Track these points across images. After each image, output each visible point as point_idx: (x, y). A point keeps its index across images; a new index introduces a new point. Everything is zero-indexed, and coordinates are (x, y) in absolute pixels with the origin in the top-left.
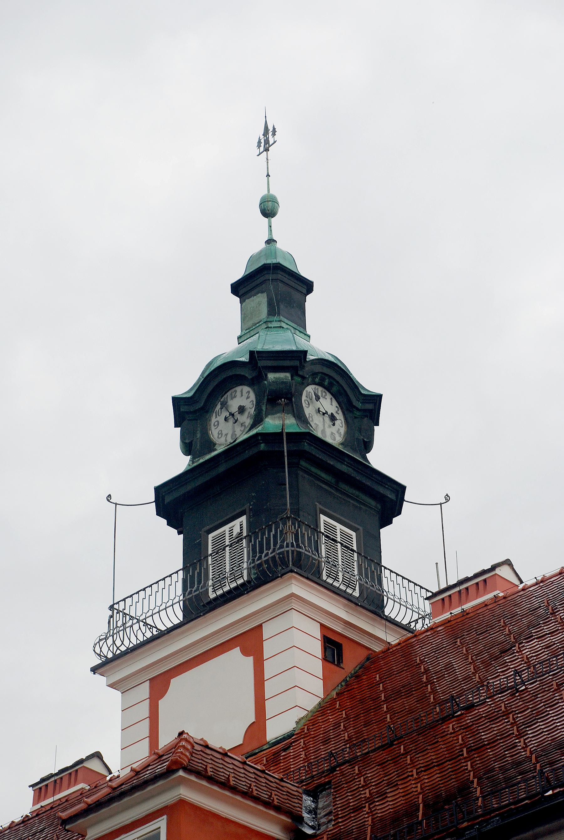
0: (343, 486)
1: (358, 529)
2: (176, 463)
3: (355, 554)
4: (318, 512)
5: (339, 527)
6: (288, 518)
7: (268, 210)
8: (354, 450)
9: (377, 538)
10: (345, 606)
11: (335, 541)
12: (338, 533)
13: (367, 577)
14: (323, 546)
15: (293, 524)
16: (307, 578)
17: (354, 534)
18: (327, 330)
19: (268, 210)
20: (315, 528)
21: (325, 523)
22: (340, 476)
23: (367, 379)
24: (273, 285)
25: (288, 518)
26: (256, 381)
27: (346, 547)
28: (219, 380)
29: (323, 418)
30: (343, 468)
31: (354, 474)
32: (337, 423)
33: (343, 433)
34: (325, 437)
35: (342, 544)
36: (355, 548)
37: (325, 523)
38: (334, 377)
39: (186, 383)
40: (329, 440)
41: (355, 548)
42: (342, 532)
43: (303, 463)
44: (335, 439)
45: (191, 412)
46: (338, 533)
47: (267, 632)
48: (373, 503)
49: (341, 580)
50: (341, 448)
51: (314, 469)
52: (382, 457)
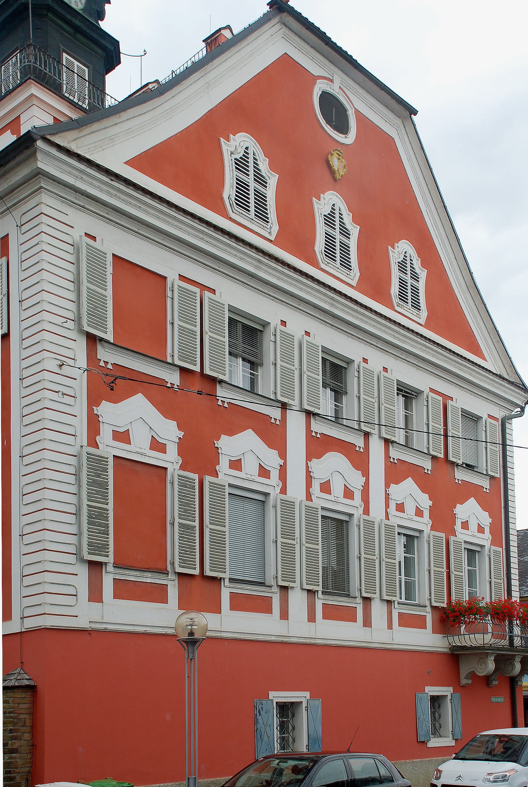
0: (78, 36)
1: (89, 67)
3: (87, 83)
4: (61, 51)
5: (76, 63)
6: (31, 45)
8: (91, 15)
9: (104, 78)
10: (69, 107)
11: (73, 72)
12: (76, 67)
13: (94, 98)
14: (64, 74)
15: (35, 49)
16: (41, 85)
17: (87, 70)
20: (60, 62)
21: (66, 58)
22: (77, 29)
25: (31, 45)
27: (80, 76)
30: (77, 23)
31: (84, 28)
32: (327, 210)
33: (83, 3)
34: (71, 3)
35: (78, 75)
36: (87, 79)
37: (66, 58)
40: (73, 6)
41: (87, 79)
42: (78, 66)
43: (50, 15)
44: (78, 6)
46: (76, 67)
47: (23, 119)
48: (100, 51)
49: (87, 104)
50: (81, 12)
51: (55, 19)
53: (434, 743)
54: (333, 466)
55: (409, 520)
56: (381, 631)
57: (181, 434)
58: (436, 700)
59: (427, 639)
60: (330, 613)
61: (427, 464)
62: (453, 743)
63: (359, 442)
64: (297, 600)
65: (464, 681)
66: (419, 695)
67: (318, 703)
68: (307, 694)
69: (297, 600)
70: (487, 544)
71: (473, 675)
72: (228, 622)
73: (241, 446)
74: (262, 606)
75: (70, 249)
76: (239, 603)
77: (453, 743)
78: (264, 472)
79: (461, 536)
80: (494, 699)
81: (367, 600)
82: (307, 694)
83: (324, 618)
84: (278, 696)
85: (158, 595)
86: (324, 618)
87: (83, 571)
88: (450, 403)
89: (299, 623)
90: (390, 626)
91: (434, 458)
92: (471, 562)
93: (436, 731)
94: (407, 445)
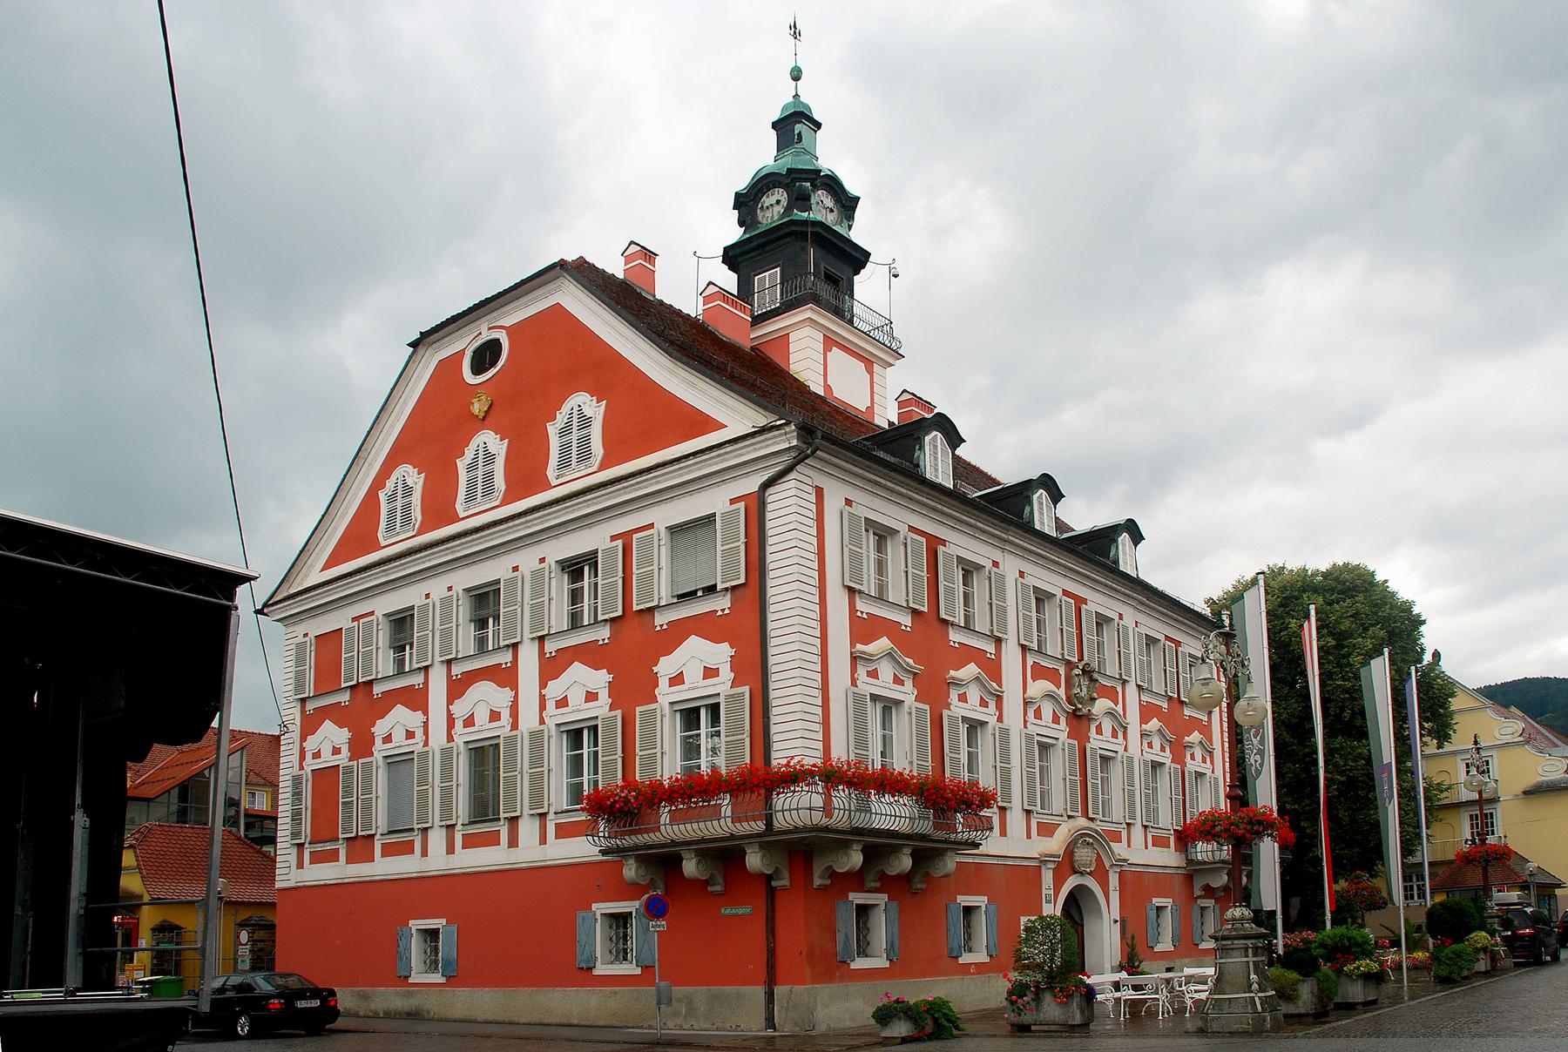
2: (735, 234)
7: (796, 75)
18: (830, 153)
19: (796, 75)
23: (851, 187)
24: (794, 125)
26: (786, 187)
28: (764, 183)
29: (822, 209)
38: (832, 185)
39: (742, 183)
45: (746, 203)
52: (859, 234)
53: (859, 964)
54: (486, 695)
55: (578, 711)
56: (533, 848)
57: (655, 669)
58: (863, 911)
59: (1168, 858)
60: (317, 858)
61: (906, 620)
62: (638, 971)
63: (990, 648)
64: (437, 838)
65: (817, 882)
66: (580, 915)
67: (454, 928)
68: (444, 921)
69: (437, 838)
70: (1063, 736)
71: (833, 875)
72: (383, 867)
73: (400, 718)
74: (407, 848)
75: (810, 489)
76: (388, 851)
77: (638, 971)
78: (410, 735)
79: (957, 709)
80: (726, 911)
81: (514, 821)
82: (444, 921)
83: (383, 856)
84: (965, 900)
85: (332, 856)
86: (383, 856)
87: (294, 851)
88: (941, 549)
89: (437, 858)
90: (543, 841)
91: (915, 612)
92: (971, 742)
93: (863, 951)
94: (881, 598)
